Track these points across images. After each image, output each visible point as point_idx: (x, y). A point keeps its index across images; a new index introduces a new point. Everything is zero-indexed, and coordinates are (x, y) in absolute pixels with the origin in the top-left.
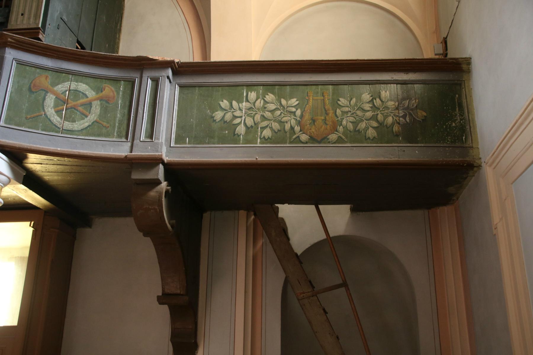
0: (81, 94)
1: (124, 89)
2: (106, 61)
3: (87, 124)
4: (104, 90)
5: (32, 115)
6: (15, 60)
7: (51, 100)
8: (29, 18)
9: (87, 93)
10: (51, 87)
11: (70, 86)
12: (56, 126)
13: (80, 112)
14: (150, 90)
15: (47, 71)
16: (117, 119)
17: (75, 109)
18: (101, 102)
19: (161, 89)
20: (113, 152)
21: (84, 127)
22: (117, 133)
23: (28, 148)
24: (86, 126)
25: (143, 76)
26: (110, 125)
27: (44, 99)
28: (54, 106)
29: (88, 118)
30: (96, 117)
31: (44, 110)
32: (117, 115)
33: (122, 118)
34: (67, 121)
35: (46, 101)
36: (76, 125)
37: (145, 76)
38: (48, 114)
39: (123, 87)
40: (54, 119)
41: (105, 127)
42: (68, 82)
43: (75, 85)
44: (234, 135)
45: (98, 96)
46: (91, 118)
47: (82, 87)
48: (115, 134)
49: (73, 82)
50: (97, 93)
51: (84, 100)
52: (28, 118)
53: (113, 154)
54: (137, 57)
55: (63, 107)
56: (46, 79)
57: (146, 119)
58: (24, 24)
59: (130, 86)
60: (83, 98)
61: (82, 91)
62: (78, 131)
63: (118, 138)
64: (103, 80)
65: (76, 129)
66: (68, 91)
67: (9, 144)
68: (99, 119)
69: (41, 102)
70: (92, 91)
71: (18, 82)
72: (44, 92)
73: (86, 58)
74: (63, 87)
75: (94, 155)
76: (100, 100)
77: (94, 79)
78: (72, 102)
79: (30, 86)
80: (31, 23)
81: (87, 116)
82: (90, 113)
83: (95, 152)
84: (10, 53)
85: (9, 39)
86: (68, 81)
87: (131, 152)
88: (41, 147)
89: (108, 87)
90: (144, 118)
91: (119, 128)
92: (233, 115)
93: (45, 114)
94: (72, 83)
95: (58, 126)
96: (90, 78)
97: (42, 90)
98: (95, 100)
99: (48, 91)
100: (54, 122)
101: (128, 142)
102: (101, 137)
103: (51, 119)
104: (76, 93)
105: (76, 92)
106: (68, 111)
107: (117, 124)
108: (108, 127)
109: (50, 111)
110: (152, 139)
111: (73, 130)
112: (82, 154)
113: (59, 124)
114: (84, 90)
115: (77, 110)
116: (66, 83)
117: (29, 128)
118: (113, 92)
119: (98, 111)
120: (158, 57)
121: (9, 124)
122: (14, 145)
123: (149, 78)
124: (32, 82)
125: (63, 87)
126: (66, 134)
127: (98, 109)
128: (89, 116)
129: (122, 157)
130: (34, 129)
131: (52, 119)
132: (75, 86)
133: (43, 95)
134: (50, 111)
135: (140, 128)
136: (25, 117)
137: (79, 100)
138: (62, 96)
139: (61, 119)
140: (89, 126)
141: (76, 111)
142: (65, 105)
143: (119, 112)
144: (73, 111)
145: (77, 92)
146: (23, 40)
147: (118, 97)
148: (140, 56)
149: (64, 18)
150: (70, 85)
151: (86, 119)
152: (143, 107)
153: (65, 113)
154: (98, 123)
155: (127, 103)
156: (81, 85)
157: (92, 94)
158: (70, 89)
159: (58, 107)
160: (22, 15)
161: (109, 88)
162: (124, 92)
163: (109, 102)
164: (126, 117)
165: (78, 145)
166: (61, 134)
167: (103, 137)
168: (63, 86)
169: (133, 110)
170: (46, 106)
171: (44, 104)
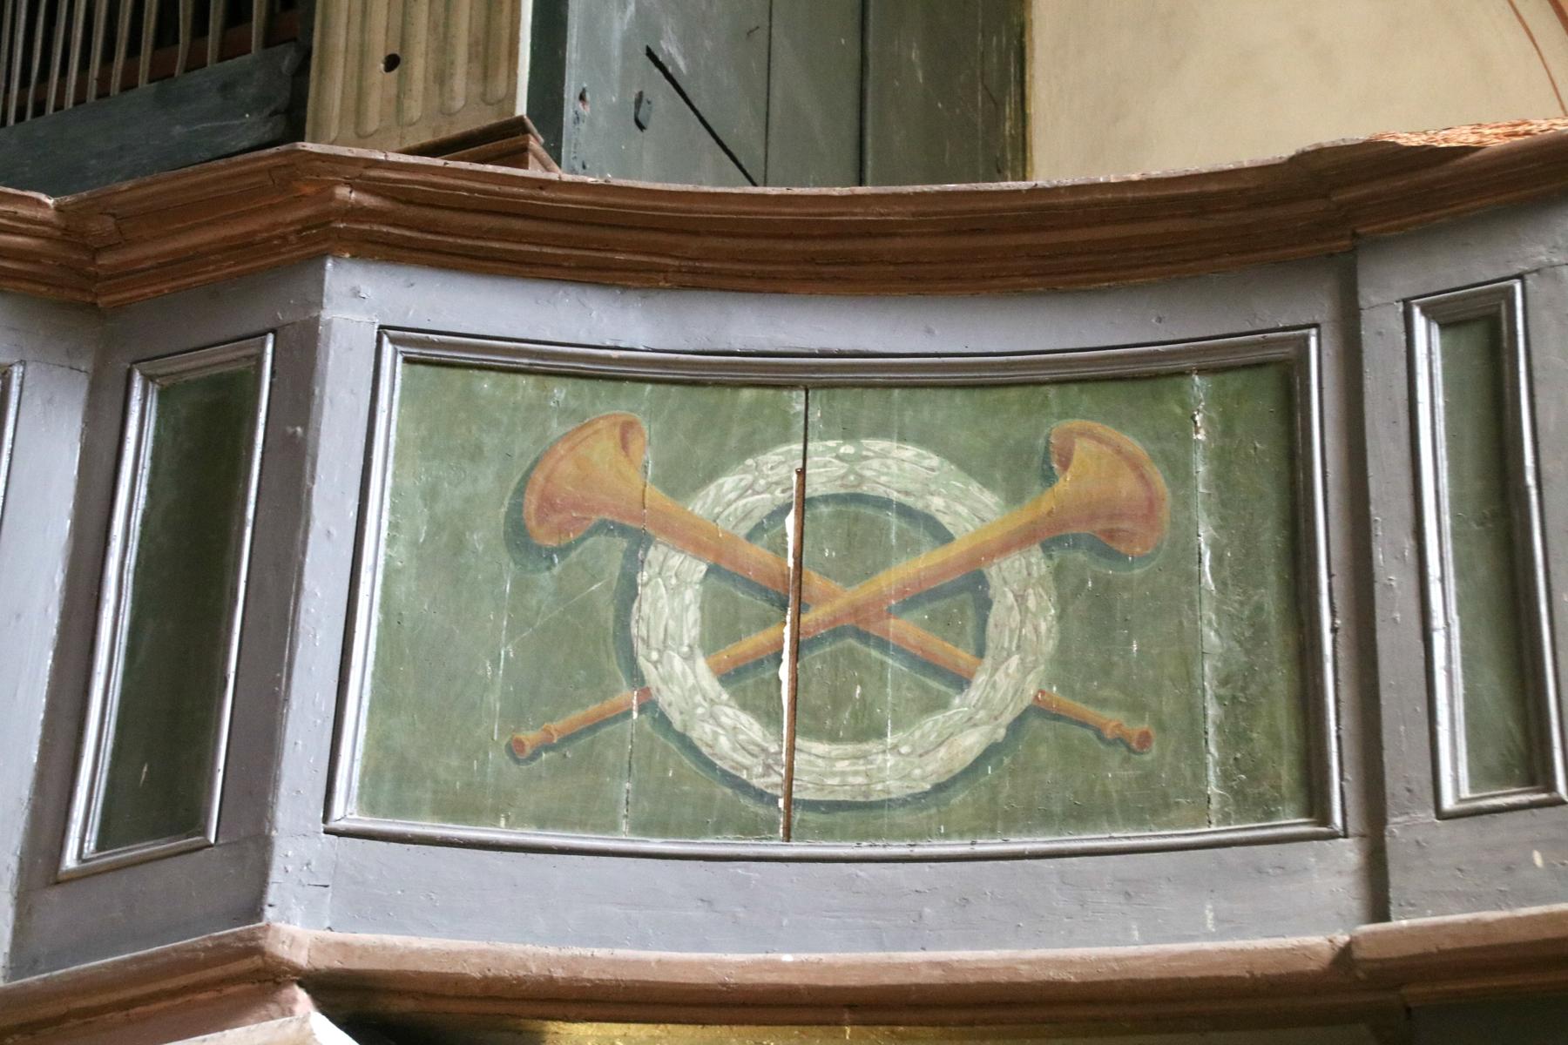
0: (892, 518)
1: (1225, 427)
2: (1053, 238)
3: (972, 742)
4: (1065, 465)
5: (558, 725)
6: (393, 341)
7: (675, 592)
8: (441, 77)
9: (937, 503)
10: (668, 502)
11: (802, 473)
12: (743, 787)
13: (902, 652)
14: (1440, 401)
15: (626, 384)
16: (1208, 670)
17: (864, 637)
18: (1056, 561)
19: (1537, 374)
20: (1221, 936)
21: (958, 767)
22: (1225, 777)
23: (551, 980)
24: (970, 759)
25: (1362, 303)
26: (1161, 726)
27: (628, 592)
28: (702, 635)
29: (974, 694)
30: (1031, 677)
31: (635, 676)
32: (1198, 635)
33: (1247, 652)
34: (818, 734)
35: (646, 608)
36: (891, 760)
37: (1374, 300)
38: (669, 698)
39: (1208, 420)
40: (715, 734)
41: (1121, 741)
42: (785, 448)
43: (838, 457)
45: (1023, 516)
46: (994, 686)
47: (895, 469)
48: (1213, 789)
49: (821, 438)
50: (1015, 496)
51: (924, 562)
52: (528, 751)
53: (1223, 951)
54: (1301, 160)
55: (772, 632)
56: (624, 445)
57: (1456, 630)
58: (412, 124)
59: (1263, 403)
60: (909, 546)
61: (895, 496)
62: (915, 801)
63: (1237, 822)
64: (1044, 389)
65: (896, 788)
66: (792, 514)
67: (409, 966)
68: (1061, 688)
69: (608, 615)
70: (974, 487)
71: (431, 494)
72: (624, 544)
73: (898, 243)
74: (750, 488)
75: (1070, 976)
76: (1046, 548)
77: (977, 393)
78: (835, 585)
79: (517, 508)
80: (459, 103)
81: (961, 682)
82: (980, 653)
83: (1077, 952)
84: (356, 293)
85: (343, 192)
86: (786, 439)
87: (1379, 909)
88: (652, 955)
89: (1084, 433)
90: (1438, 621)
91: (1234, 736)
93: (648, 705)
94: (811, 446)
95: (757, 783)
96: (943, 394)
97: (603, 527)
98: (1006, 547)
99: (651, 531)
100: (722, 758)
101: (1333, 836)
102: (1096, 827)
103: (694, 735)
104: (857, 518)
105: (852, 508)
106: (815, 660)
107: (1213, 711)
108: (1145, 739)
109: (684, 674)
110: (1550, 786)
111: (874, 798)
112: (972, 979)
113: (760, 770)
114: (911, 487)
115: (883, 645)
116: (772, 457)
117: (541, 823)
118: (1136, 466)
119: (1043, 627)
120: (1467, 130)
121: (399, 809)
122: (447, 968)
123: (1417, 311)
124: (526, 478)
125: (750, 488)
126: (826, 833)
127: (1042, 610)
128: (980, 679)
129: (1313, 966)
130: (582, 825)
131: (701, 733)
132: (839, 468)
133: (615, 569)
134: (684, 674)
135: (1422, 709)
136: (504, 743)
137: (885, 565)
138: (757, 554)
139: (766, 726)
140: (991, 752)
141: (875, 653)
142: (788, 619)
143: (1209, 613)
144: (851, 650)
145: (869, 511)
146: (436, 179)
147: (1185, 503)
148: (1320, 152)
149: (670, 49)
150: (799, 465)
151: (957, 701)
152: (1408, 544)
153: (795, 679)
154: (1057, 717)
155: (1270, 537)
156: (883, 455)
157: (974, 511)
158: (809, 492)
159: (736, 638)
160: (392, 62)
161: (1099, 440)
162: (1223, 460)
163: (1114, 545)
164: (1277, 644)
165: (927, 910)
166: (788, 837)
167: (1113, 824)
168: (755, 481)
169: (1330, 576)
170: (647, 642)
171: (634, 631)
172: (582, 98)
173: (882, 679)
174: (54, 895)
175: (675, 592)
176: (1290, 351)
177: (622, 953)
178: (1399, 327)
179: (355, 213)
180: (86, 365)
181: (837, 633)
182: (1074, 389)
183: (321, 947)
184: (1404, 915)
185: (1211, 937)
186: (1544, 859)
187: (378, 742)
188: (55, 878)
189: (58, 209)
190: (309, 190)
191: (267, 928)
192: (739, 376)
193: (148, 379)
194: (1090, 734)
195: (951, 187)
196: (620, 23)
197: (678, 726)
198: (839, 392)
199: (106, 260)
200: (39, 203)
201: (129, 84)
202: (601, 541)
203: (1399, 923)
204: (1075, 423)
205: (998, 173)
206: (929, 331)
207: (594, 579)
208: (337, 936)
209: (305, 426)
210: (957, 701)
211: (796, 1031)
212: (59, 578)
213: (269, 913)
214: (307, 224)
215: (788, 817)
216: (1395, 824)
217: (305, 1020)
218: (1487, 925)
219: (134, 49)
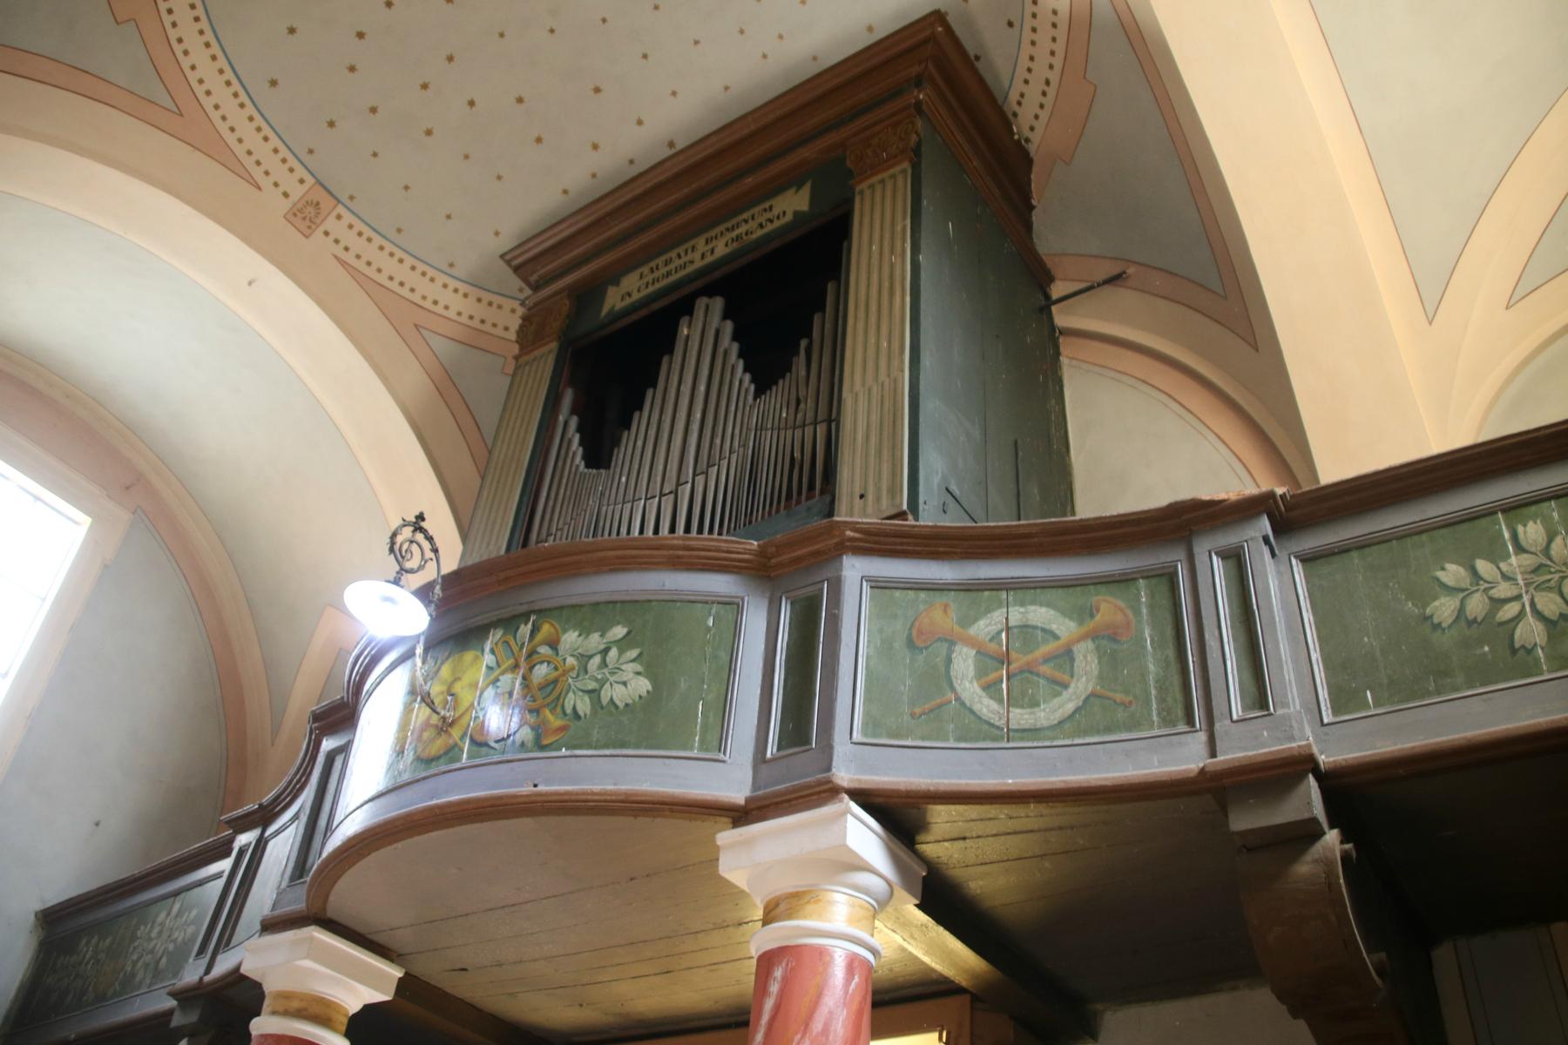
0: (1039, 632)
1: (1152, 596)
3: (1070, 707)
4: (1098, 611)
6: (866, 581)
7: (965, 660)
8: (878, 499)
9: (1054, 627)
10: (961, 630)
11: (1007, 619)
12: (992, 725)
17: (1031, 672)
21: (1066, 715)
22: (1159, 714)
23: (929, 791)
24: (1070, 712)
27: (949, 661)
29: (1071, 690)
31: (953, 689)
34: (1013, 706)
36: (1042, 714)
38: (965, 696)
39: (1146, 594)
41: (1123, 703)
44: (1514, 651)
46: (1078, 687)
50: (1081, 622)
51: (1051, 646)
52: (918, 715)
53: (1161, 772)
55: (999, 672)
56: (945, 611)
59: (1164, 587)
60: (1045, 641)
61: (1040, 625)
62: (1052, 728)
65: (1045, 723)
67: (881, 786)
70: (1067, 621)
71: (881, 631)
72: (946, 645)
77: (1066, 589)
78: (1021, 656)
79: (910, 634)
81: (1065, 686)
82: (1072, 676)
83: (1110, 775)
84: (853, 566)
86: (1000, 606)
87: (1213, 754)
88: (963, 782)
92: (1491, 599)
93: (958, 699)
94: (1009, 610)
95: (997, 723)
96: (1054, 590)
97: (939, 639)
101: (1197, 731)
105: (1025, 630)
106: (1015, 681)
107: (1153, 692)
108: (1130, 702)
110: (1268, 709)
115: (1038, 675)
117: (923, 739)
118: (1122, 610)
119: (1093, 666)
121: (875, 735)
123: (1213, 554)
124: (912, 625)
125: (990, 624)
126: (1022, 739)
128: (1073, 685)
129: (1192, 775)
130: (937, 739)
131: (976, 707)
132: (1019, 616)
138: (993, 646)
140: (1077, 710)
141: (1035, 678)
143: (1150, 658)
145: (1030, 630)
148: (1176, 503)
149: (954, 488)
152: (1217, 633)
155: (1169, 632)
156: (1035, 611)
158: (1010, 625)
159: (987, 675)
160: (862, 496)
162: (1151, 607)
164: (1174, 667)
167: (1121, 732)
170: (956, 678)
171: (952, 674)
172: (925, 503)
173: (1038, 686)
174: (764, 766)
175: (965, 660)
176: (1171, 570)
177: (953, 781)
178: (1208, 559)
179: (852, 539)
180: (767, 595)
181: (1021, 672)
182: (1099, 586)
183: (852, 780)
184: (1222, 755)
185: (1157, 767)
186: (1268, 734)
187: (867, 714)
188: (764, 761)
189: (759, 546)
190: (837, 533)
191: (833, 775)
192: (984, 587)
193: (787, 599)
194: (1112, 702)
195: (1053, 520)
196: (936, 480)
197: (968, 703)
198: (1018, 591)
199: (774, 561)
200: (752, 544)
201: (778, 511)
202: (939, 644)
203: (1220, 758)
204: (1099, 598)
205: (1065, 515)
206: (1049, 569)
207: (937, 657)
208: (856, 777)
209: (839, 610)
210: (1065, 693)
211: (1014, 806)
212: (761, 665)
213: (834, 770)
214: (837, 544)
215: (1008, 735)
216: (1217, 726)
217: (848, 804)
218: (1250, 757)
219: (779, 502)
